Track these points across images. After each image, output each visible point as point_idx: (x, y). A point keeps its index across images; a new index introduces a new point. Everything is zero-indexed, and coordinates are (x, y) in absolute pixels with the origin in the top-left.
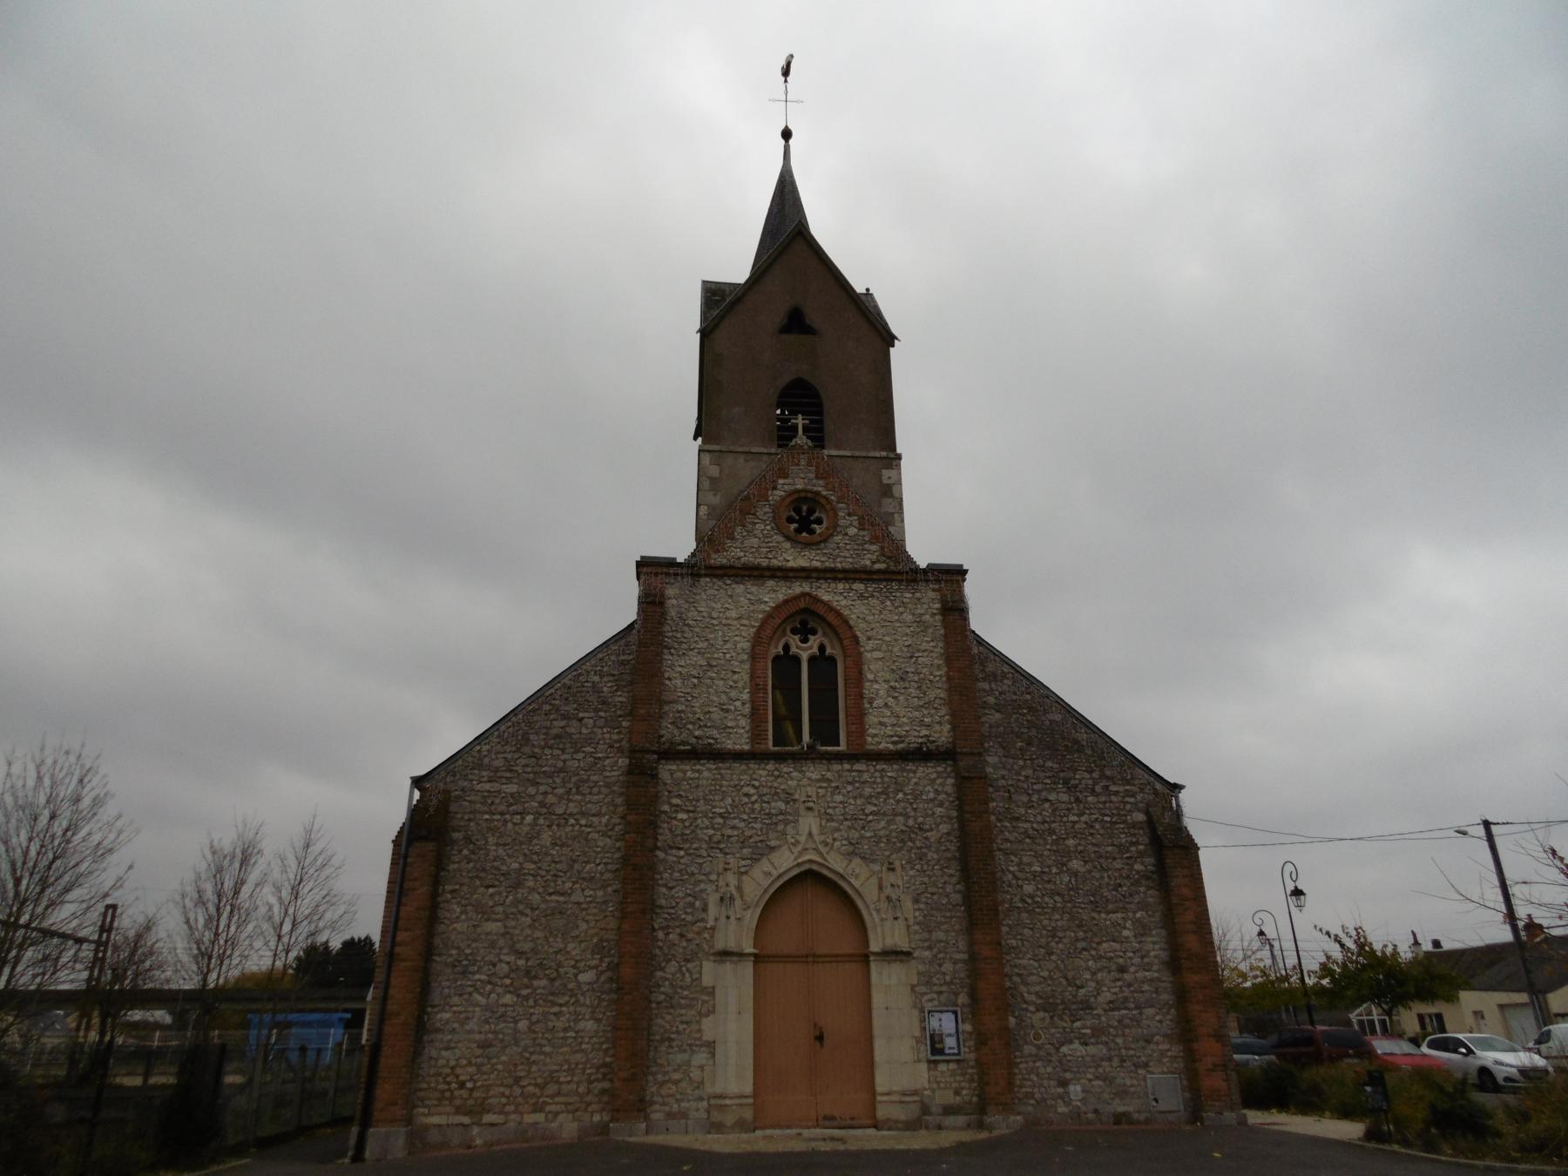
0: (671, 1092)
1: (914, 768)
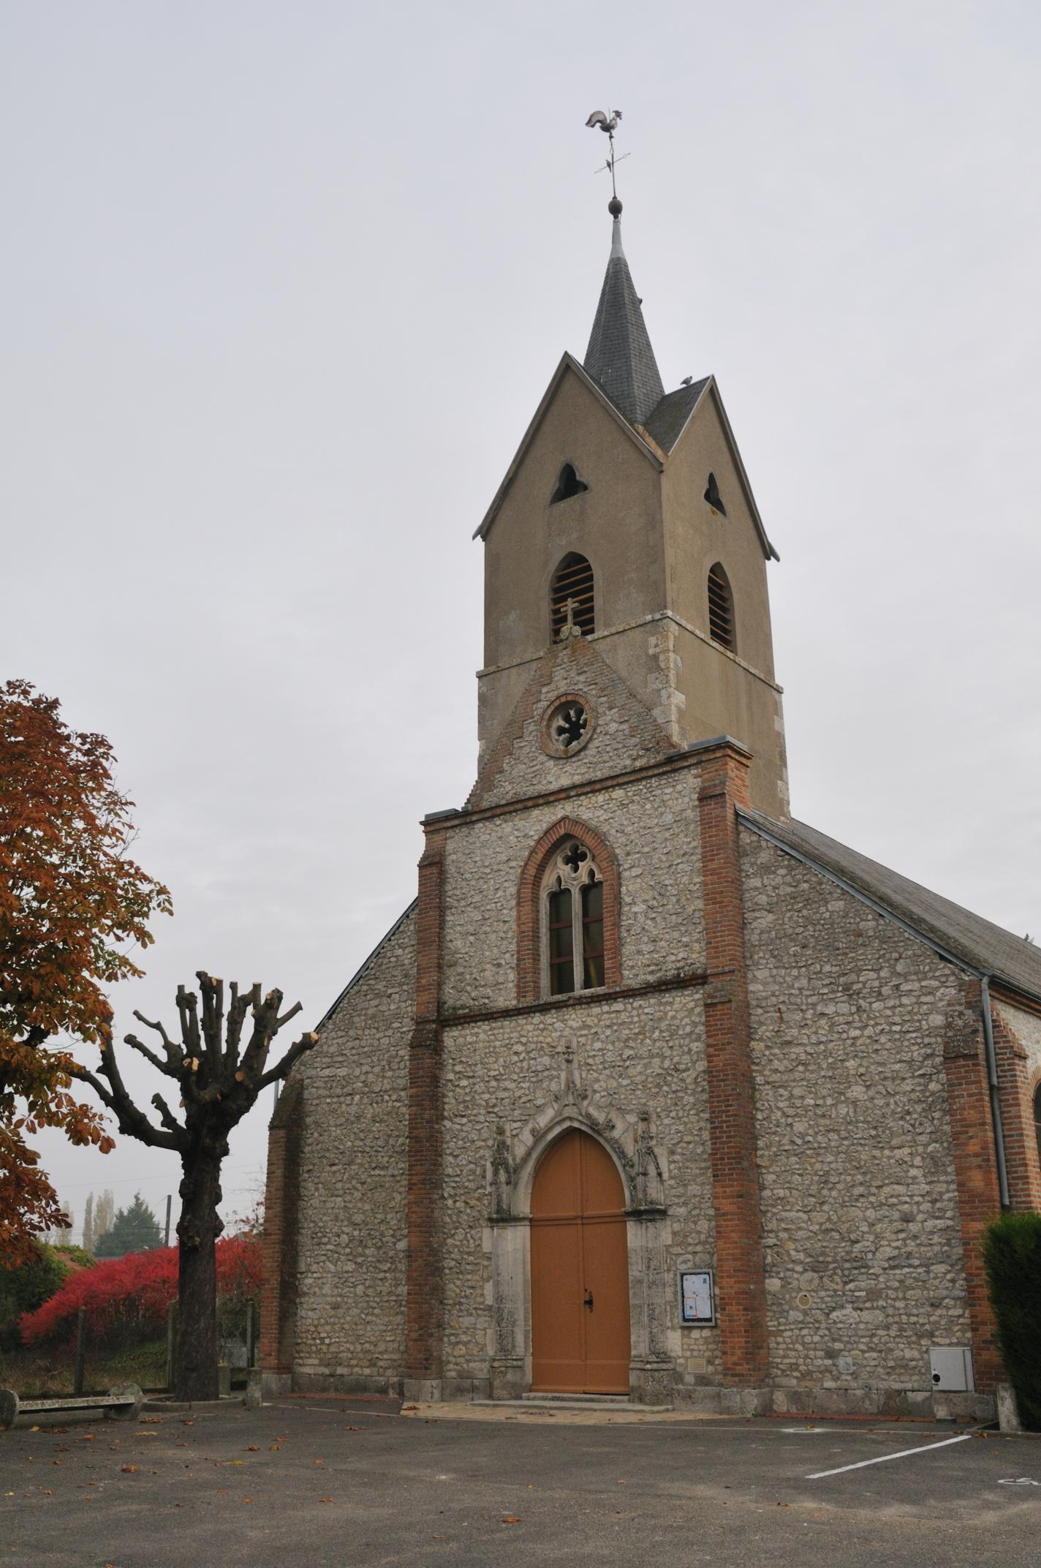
0: (462, 1352)
1: (671, 1000)
